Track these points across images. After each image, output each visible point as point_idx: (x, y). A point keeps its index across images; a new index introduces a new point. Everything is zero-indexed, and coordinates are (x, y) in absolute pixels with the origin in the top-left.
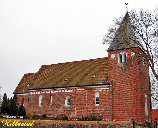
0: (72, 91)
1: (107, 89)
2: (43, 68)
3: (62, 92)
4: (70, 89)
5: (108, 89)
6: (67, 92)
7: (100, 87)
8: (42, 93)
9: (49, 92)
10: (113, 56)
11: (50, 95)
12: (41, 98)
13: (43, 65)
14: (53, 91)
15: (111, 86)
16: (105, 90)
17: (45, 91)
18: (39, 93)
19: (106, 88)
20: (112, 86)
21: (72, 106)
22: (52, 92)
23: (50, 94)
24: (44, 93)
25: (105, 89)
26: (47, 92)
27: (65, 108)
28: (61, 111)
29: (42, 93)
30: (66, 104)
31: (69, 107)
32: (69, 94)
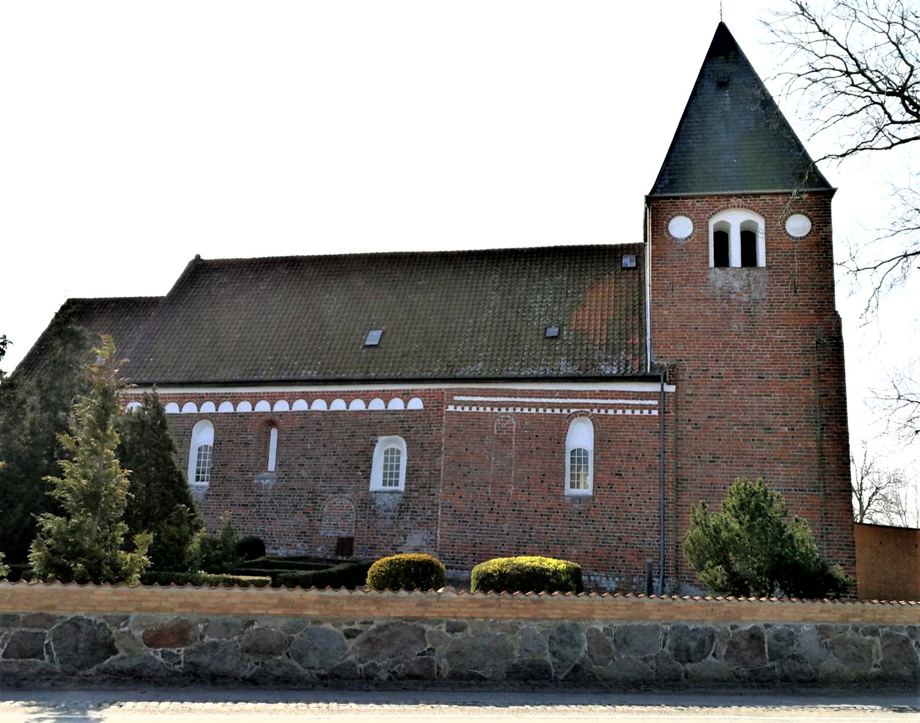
0: (416, 404)
1: (643, 407)
2: (199, 272)
3: (275, 409)
4: (406, 397)
5: (651, 408)
6: (387, 412)
7: (603, 394)
8: (208, 407)
9: (263, 406)
10: (681, 227)
11: (271, 421)
12: (203, 436)
13: (198, 257)
14: (291, 399)
15: (671, 389)
16: (611, 412)
17: (367, 398)
18: (190, 408)
19: (637, 399)
20: (675, 394)
21: (416, 494)
22: (281, 406)
23: (268, 418)
24: (226, 407)
25: (633, 408)
26: (245, 407)
27: (367, 503)
28: (336, 518)
29: (208, 407)
30: (376, 483)
31: (397, 496)
32: (399, 423)
